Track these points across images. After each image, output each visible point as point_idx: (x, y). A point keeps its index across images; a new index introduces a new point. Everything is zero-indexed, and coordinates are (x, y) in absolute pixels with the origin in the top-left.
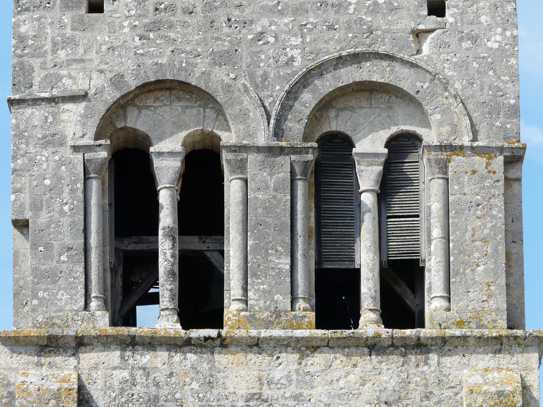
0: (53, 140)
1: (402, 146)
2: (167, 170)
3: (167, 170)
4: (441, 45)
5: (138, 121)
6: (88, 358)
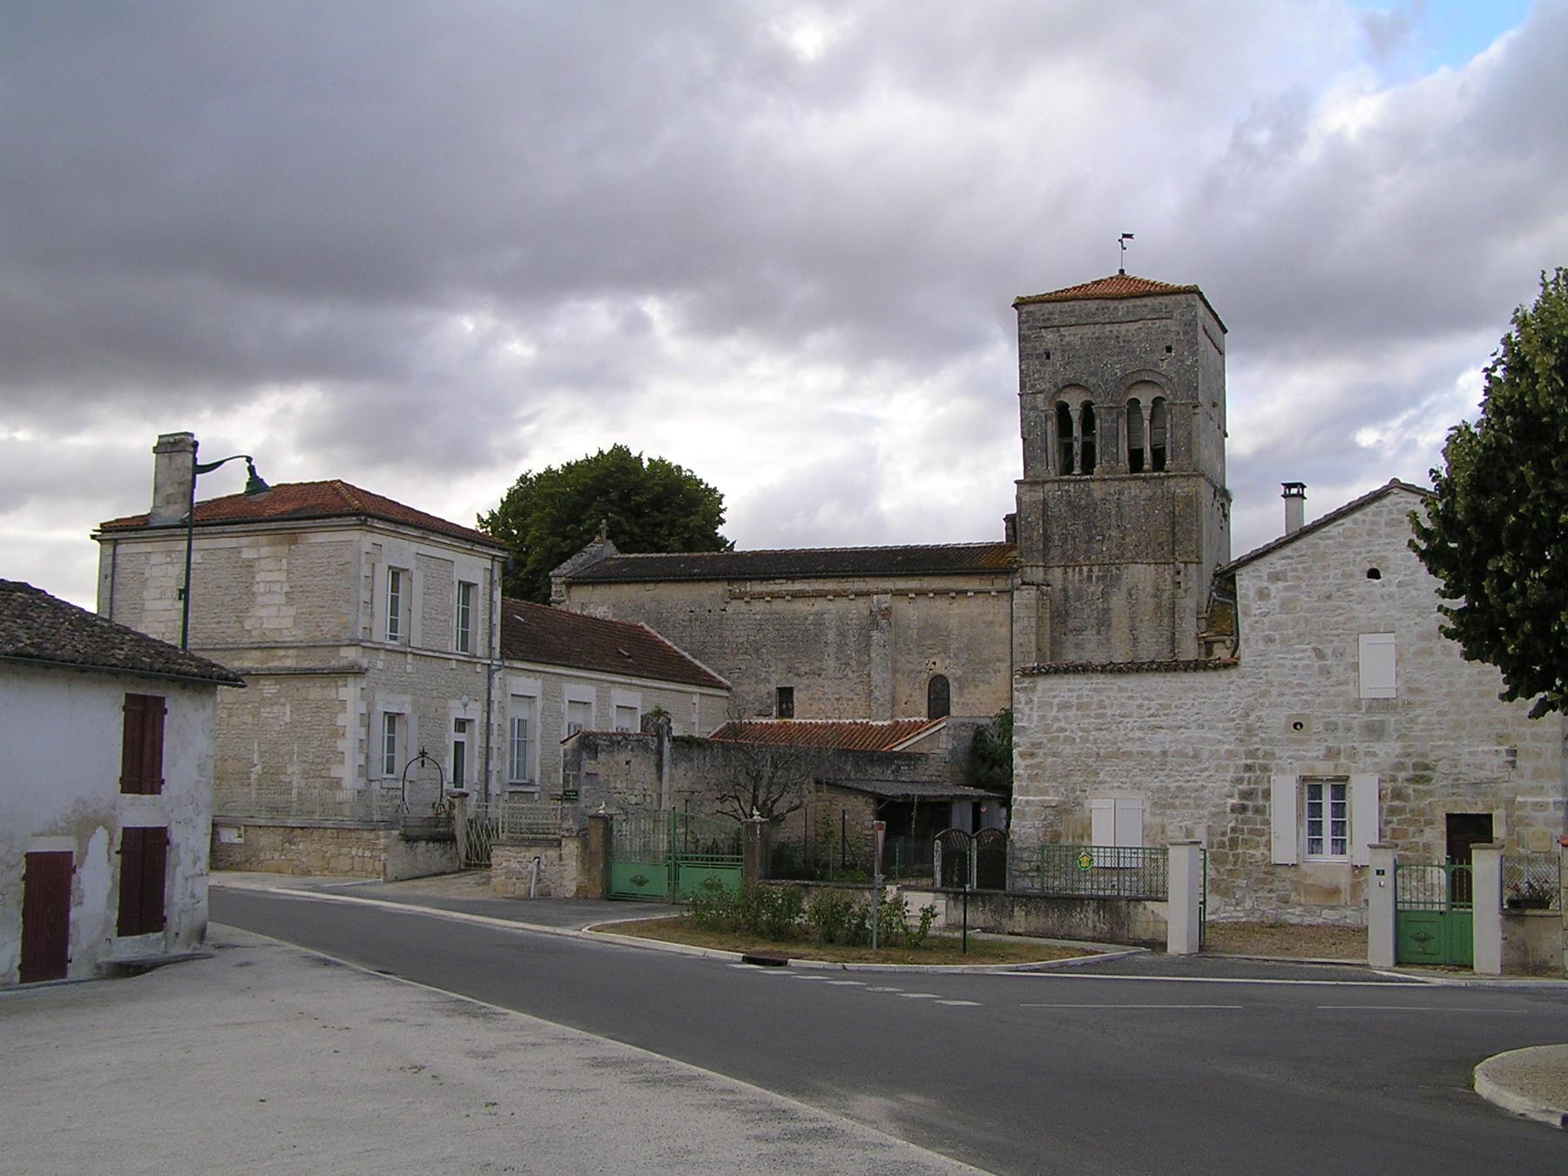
0: (1034, 408)
1: (1157, 402)
2: (1075, 415)
3: (1075, 415)
4: (1170, 364)
5: (1064, 398)
6: (1048, 486)
